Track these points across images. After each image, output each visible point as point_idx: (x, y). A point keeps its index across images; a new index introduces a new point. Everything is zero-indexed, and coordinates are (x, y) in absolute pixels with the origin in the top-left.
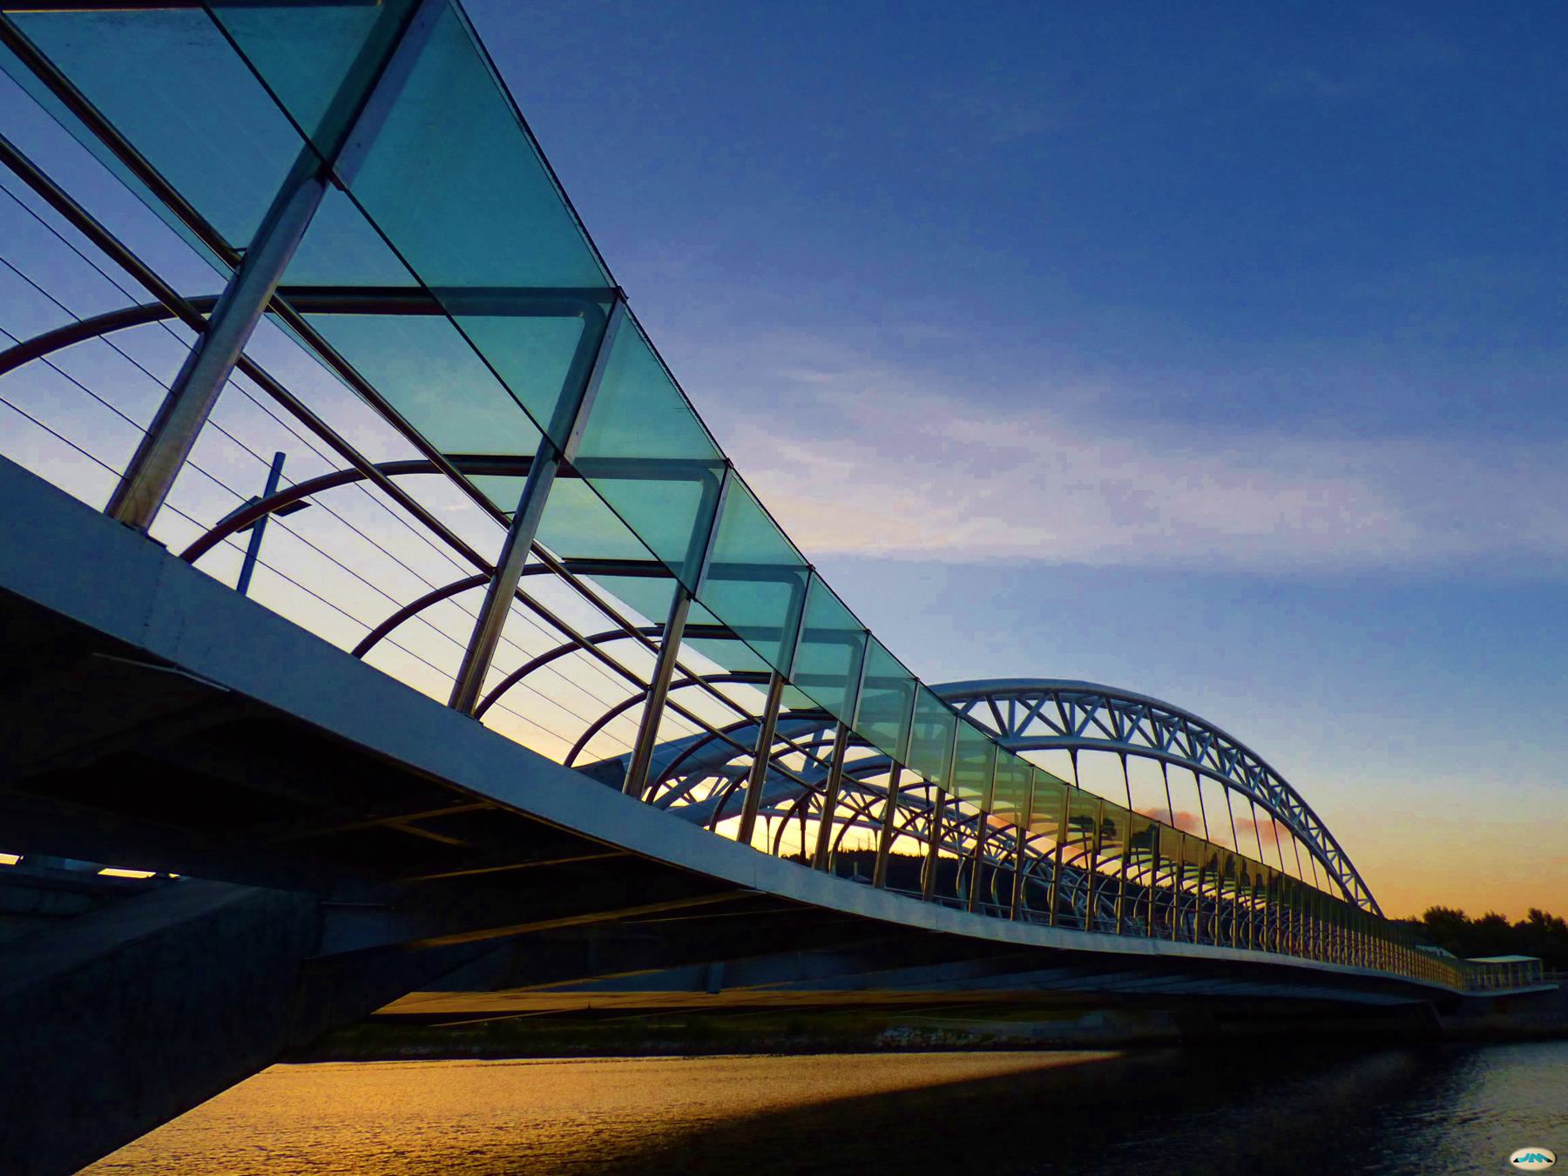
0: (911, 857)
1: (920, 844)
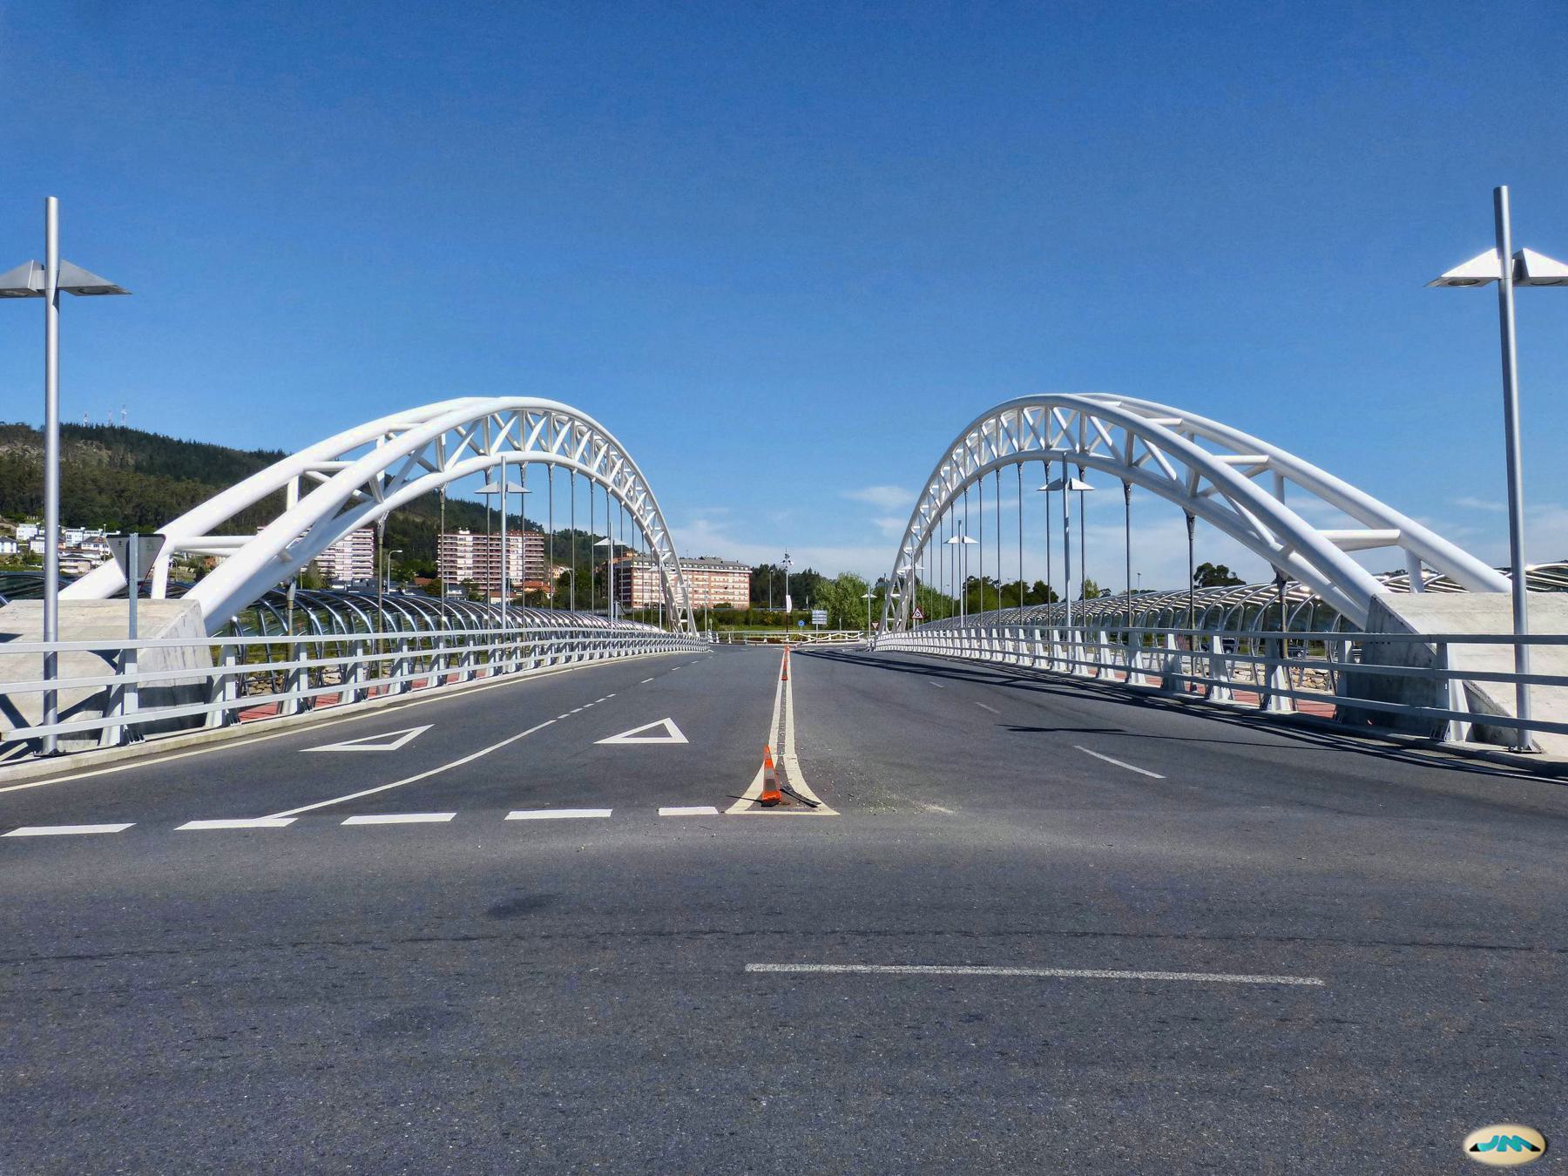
0: (180, 442)
1: (1190, 520)
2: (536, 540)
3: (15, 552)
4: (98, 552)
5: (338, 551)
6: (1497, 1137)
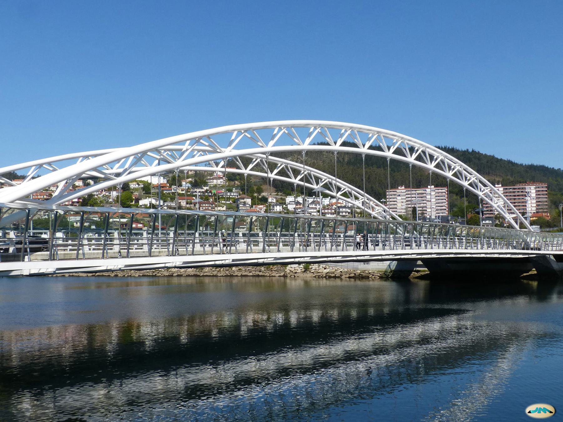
0: (548, 167)
2: (542, 187)
3: (281, 210)
4: (316, 208)
5: (428, 201)
6: (538, 408)
